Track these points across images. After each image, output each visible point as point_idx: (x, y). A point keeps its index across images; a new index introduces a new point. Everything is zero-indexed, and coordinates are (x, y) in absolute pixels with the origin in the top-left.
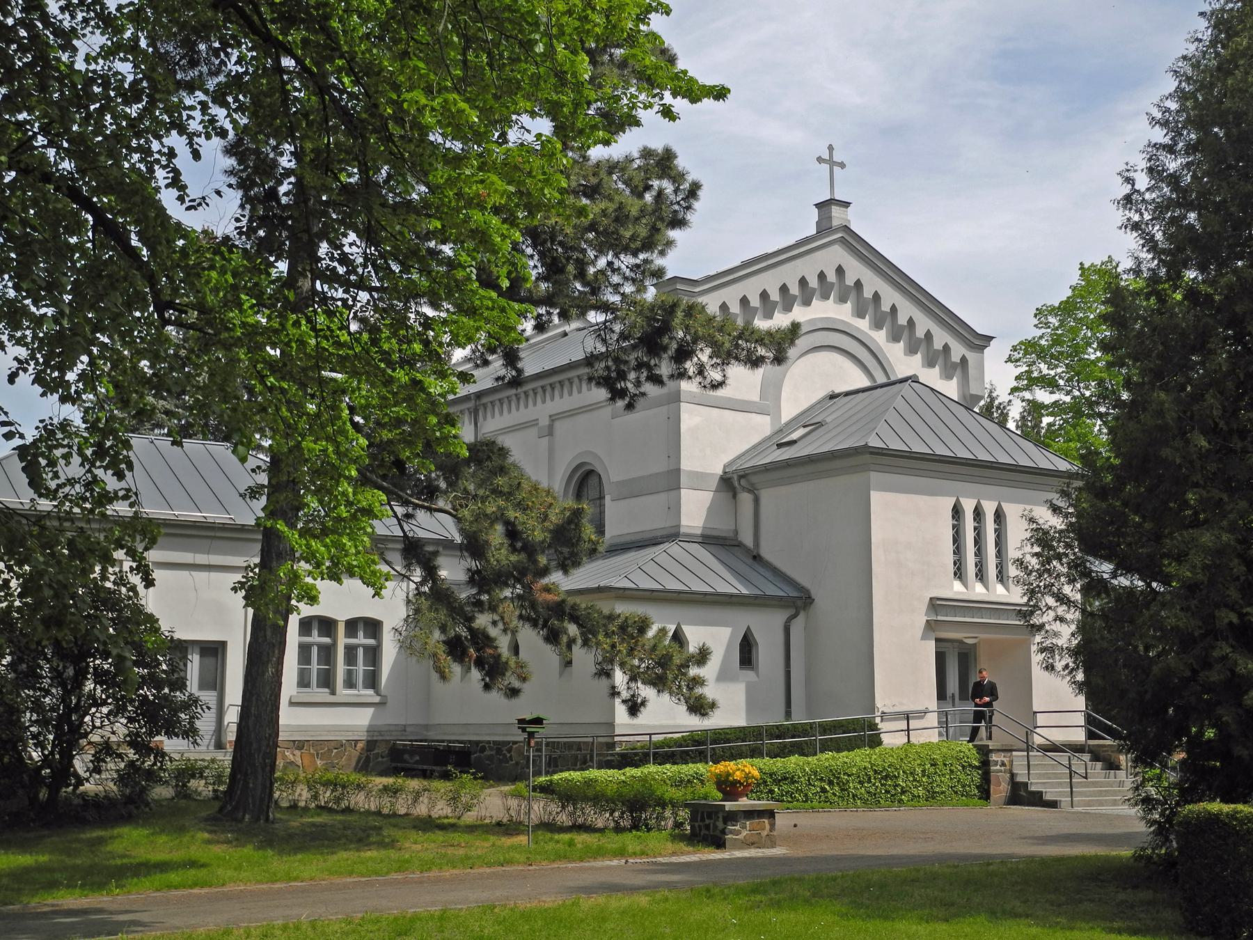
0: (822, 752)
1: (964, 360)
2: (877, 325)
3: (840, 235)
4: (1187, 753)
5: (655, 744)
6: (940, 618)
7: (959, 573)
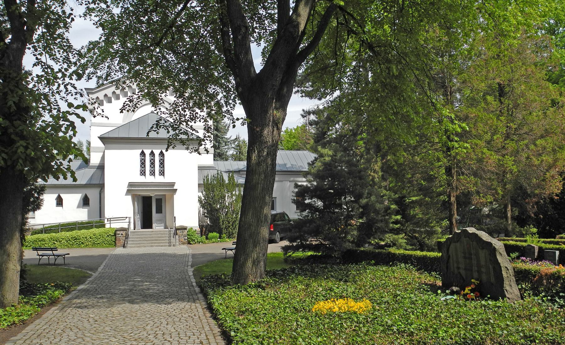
7: (143, 173)
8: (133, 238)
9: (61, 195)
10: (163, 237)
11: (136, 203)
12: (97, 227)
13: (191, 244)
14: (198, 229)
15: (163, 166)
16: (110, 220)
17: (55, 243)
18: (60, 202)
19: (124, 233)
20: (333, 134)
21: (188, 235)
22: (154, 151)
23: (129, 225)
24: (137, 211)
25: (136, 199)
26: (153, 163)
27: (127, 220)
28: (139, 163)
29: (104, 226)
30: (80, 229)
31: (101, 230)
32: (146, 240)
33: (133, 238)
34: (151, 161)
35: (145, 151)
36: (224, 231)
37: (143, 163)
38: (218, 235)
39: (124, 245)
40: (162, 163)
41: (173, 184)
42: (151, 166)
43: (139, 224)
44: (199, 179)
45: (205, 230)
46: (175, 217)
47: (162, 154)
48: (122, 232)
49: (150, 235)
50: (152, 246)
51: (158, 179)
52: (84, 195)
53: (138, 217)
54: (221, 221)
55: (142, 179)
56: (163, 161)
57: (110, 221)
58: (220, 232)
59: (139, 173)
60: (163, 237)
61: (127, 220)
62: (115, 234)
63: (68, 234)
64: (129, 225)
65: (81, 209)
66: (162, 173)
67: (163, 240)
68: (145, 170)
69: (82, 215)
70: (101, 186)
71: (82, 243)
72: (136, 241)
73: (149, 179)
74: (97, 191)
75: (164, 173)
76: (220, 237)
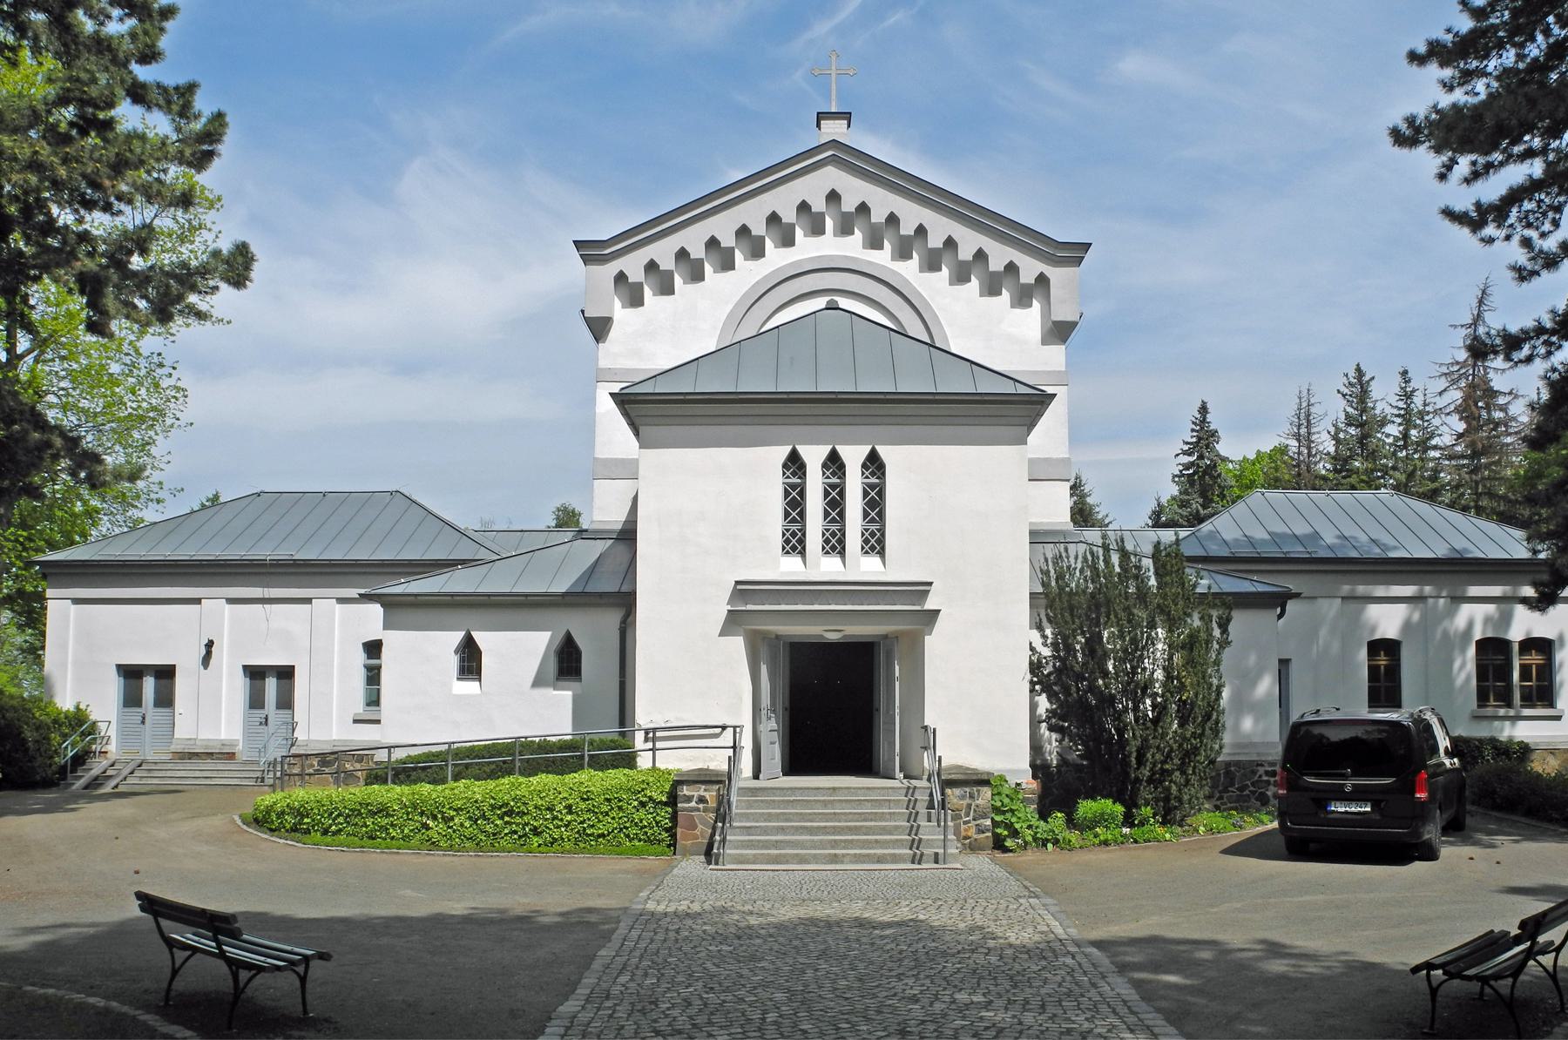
1: (1042, 280)
3: (830, 153)
4: (1282, 816)
6: (750, 607)
7: (795, 543)
8: (746, 817)
9: (475, 635)
10: (882, 817)
11: (764, 669)
12: (599, 764)
13: (1006, 850)
15: (881, 515)
16: (651, 734)
17: (427, 828)
18: (470, 661)
19: (710, 794)
20: (85, 503)
21: (997, 810)
22: (843, 450)
23: (733, 761)
24: (766, 700)
25: (764, 652)
26: (835, 503)
27: (727, 738)
28: (777, 504)
29: (629, 761)
30: (531, 769)
31: (616, 776)
32: (811, 831)
33: (746, 817)
34: (866, 494)
36: (1146, 793)
37: (795, 504)
38: (1119, 809)
39: (710, 846)
40: (875, 503)
41: (920, 590)
42: (827, 514)
43: (774, 755)
45: (1058, 790)
47: (874, 464)
48: (701, 791)
49: (825, 804)
50: (835, 859)
51: (868, 568)
53: (773, 724)
54: (1133, 748)
55: (790, 568)
56: (881, 494)
57: (654, 740)
58: (1130, 804)
59: (779, 541)
60: (882, 817)
61: (727, 738)
62: (673, 799)
63: (479, 789)
64: (733, 761)
66: (875, 544)
67: (884, 830)
68: (882, 531)
69: (552, 715)
70: (626, 601)
72: (765, 831)
73: (828, 568)
74: (613, 618)
76: (1128, 820)
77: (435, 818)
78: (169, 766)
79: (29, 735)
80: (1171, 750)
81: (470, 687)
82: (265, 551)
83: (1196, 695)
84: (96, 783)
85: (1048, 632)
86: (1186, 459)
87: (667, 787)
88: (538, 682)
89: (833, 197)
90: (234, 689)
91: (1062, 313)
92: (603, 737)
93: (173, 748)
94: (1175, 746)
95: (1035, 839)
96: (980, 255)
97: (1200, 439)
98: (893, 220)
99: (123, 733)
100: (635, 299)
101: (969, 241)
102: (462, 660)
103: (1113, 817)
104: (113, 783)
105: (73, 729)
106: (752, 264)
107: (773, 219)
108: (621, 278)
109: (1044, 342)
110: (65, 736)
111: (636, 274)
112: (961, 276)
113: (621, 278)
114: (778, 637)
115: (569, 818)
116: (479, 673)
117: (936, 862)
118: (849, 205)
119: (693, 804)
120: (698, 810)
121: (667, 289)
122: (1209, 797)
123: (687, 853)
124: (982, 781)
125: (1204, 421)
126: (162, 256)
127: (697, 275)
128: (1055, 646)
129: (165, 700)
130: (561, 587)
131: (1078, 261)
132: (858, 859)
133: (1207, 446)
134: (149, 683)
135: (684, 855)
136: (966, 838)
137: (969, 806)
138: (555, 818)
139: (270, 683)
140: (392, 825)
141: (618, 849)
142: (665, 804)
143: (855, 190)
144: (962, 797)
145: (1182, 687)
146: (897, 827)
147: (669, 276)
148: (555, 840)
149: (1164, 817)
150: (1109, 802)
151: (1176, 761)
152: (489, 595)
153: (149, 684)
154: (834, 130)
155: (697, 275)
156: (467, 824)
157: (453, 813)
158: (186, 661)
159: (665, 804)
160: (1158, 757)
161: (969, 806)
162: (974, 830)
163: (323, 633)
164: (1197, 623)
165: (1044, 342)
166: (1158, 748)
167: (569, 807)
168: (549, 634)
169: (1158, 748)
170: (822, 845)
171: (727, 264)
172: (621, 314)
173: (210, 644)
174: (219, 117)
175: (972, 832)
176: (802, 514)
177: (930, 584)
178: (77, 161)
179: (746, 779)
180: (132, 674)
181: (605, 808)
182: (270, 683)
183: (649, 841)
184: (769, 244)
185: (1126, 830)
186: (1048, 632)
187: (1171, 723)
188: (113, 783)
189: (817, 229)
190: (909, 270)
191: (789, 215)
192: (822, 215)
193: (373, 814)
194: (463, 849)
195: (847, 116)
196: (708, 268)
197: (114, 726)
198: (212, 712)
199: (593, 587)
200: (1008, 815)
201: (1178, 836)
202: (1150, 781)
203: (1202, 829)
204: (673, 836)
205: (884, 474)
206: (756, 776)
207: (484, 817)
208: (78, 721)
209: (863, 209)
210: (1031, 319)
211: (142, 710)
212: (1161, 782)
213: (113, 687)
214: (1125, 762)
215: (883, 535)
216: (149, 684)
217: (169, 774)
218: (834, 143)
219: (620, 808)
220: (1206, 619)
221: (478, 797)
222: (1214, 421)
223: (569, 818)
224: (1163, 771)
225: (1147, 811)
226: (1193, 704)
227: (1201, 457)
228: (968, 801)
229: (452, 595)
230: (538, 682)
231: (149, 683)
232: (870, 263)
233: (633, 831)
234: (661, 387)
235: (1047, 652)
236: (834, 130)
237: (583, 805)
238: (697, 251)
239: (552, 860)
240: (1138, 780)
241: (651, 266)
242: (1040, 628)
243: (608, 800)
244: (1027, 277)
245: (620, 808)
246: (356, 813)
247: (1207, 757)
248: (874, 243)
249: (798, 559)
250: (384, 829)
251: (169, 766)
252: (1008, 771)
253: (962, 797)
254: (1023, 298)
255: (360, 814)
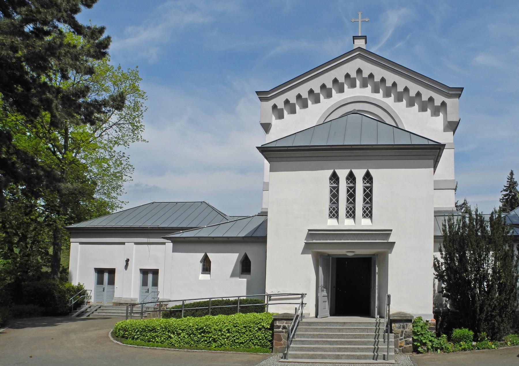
0: (185, 316)
1: (444, 104)
2: (387, 95)
3: (358, 53)
5: (187, 305)
6: (314, 241)
7: (334, 213)
10: (363, 336)
11: (320, 269)
13: (419, 352)
14: (431, 319)
15: (371, 200)
16: (270, 296)
17: (170, 337)
18: (207, 267)
21: (414, 333)
24: (321, 283)
26: (351, 196)
34: (365, 191)
35: (339, 172)
38: (471, 333)
40: (368, 195)
41: (387, 233)
43: (326, 307)
44: (435, 230)
45: (448, 321)
46: (389, 297)
47: (368, 177)
48: (284, 323)
49: (339, 330)
50: (338, 357)
51: (365, 223)
52: (243, 255)
53: (325, 293)
54: (478, 304)
55: (332, 224)
56: (371, 191)
58: (477, 332)
59: (328, 212)
60: (363, 336)
63: (191, 321)
65: (238, 279)
66: (368, 213)
69: (237, 289)
71: (215, 341)
72: (310, 343)
73: (348, 224)
75: (371, 212)
76: (475, 339)
77: (174, 333)
78: (111, 308)
79: (56, 294)
80: (495, 306)
81: (206, 277)
82: (149, 224)
83: (507, 280)
84: (82, 313)
85: (444, 253)
86: (505, 193)
87: (270, 322)
88: (233, 275)
89: (359, 71)
90: (136, 278)
91: (453, 118)
92: (252, 298)
93: (114, 301)
94: (497, 304)
95: (432, 347)
96: (419, 94)
97: (510, 185)
98: (383, 80)
99: (97, 295)
100: (281, 116)
101: (414, 88)
102: (204, 265)
103: (468, 336)
104: (88, 314)
105: (76, 293)
106: (327, 100)
107: (335, 81)
108: (275, 107)
109: (445, 130)
110: (72, 296)
111: (280, 105)
112: (411, 104)
113: (275, 107)
114: (329, 255)
115: (228, 335)
116: (210, 271)
117: (384, 359)
118: (365, 75)
119: (281, 329)
120: (283, 332)
121: (293, 111)
122: (512, 328)
123: (277, 351)
124: (408, 320)
125: (512, 178)
126: (91, 97)
127: (305, 106)
128: (445, 258)
129: (112, 282)
130: (243, 234)
131: (459, 96)
132: (349, 357)
133: (513, 188)
134: (106, 275)
135: (276, 352)
136: (400, 347)
137: (402, 332)
138: (222, 335)
139: (150, 275)
140: (157, 336)
141: (249, 350)
142: (269, 329)
143: (368, 68)
144: (400, 328)
145: (500, 278)
146: (368, 342)
147: (294, 106)
148: (222, 345)
149: (491, 337)
150: (467, 330)
151: (497, 311)
152: (213, 238)
153: (106, 276)
154: (360, 43)
155: (305, 106)
156: (186, 337)
157: (180, 331)
158: (119, 267)
159: (269, 329)
160: (489, 309)
161: (402, 332)
162: (404, 343)
163: (158, 254)
164: (507, 248)
165: (445, 130)
166: (489, 305)
167: (228, 330)
168: (238, 254)
169: (489, 305)
170: (334, 350)
171: (317, 101)
172: (275, 122)
173: (127, 261)
174: (108, 39)
175: (403, 344)
176: (337, 200)
177: (391, 230)
178: (32, 47)
179: (312, 318)
180: (100, 272)
181: (244, 331)
182: (150, 275)
183: (262, 346)
184: (334, 92)
185: (474, 343)
186: (444, 253)
187: (495, 294)
188: (88, 314)
189: (353, 85)
190: (390, 101)
191: (341, 79)
192: (355, 79)
193: (150, 331)
194: (183, 348)
195: (364, 37)
196: (309, 102)
197: (93, 292)
198: (128, 288)
199: (254, 235)
200: (420, 336)
201: (498, 346)
202: (486, 320)
203: (509, 343)
204: (272, 344)
205: (372, 182)
206: (316, 317)
207: (193, 333)
208: (80, 291)
209: (371, 76)
210: (439, 121)
211: (103, 286)
212: (491, 320)
213: (93, 276)
214: (475, 311)
215: (372, 209)
216: (106, 276)
217: (110, 311)
218: (359, 49)
219: (250, 331)
220: (511, 246)
221: (191, 324)
222: (516, 178)
223: (228, 335)
224: (491, 315)
225: (484, 334)
226: (505, 285)
227: (511, 192)
228: (402, 329)
229: (199, 238)
230: (233, 275)
231: (106, 275)
232: (375, 99)
233: (255, 341)
234: (278, 144)
235: (442, 261)
236: (360, 43)
237: (234, 329)
238: (305, 95)
239: (219, 354)
240: (480, 320)
241: (287, 102)
242: (440, 251)
243: (245, 327)
244: (438, 102)
245: (250, 331)
246: (143, 330)
247: (511, 309)
248: (376, 90)
249: (336, 220)
250: (154, 338)
251: (111, 308)
252: (424, 315)
253: (400, 328)
254: (436, 112)
255: (145, 331)
